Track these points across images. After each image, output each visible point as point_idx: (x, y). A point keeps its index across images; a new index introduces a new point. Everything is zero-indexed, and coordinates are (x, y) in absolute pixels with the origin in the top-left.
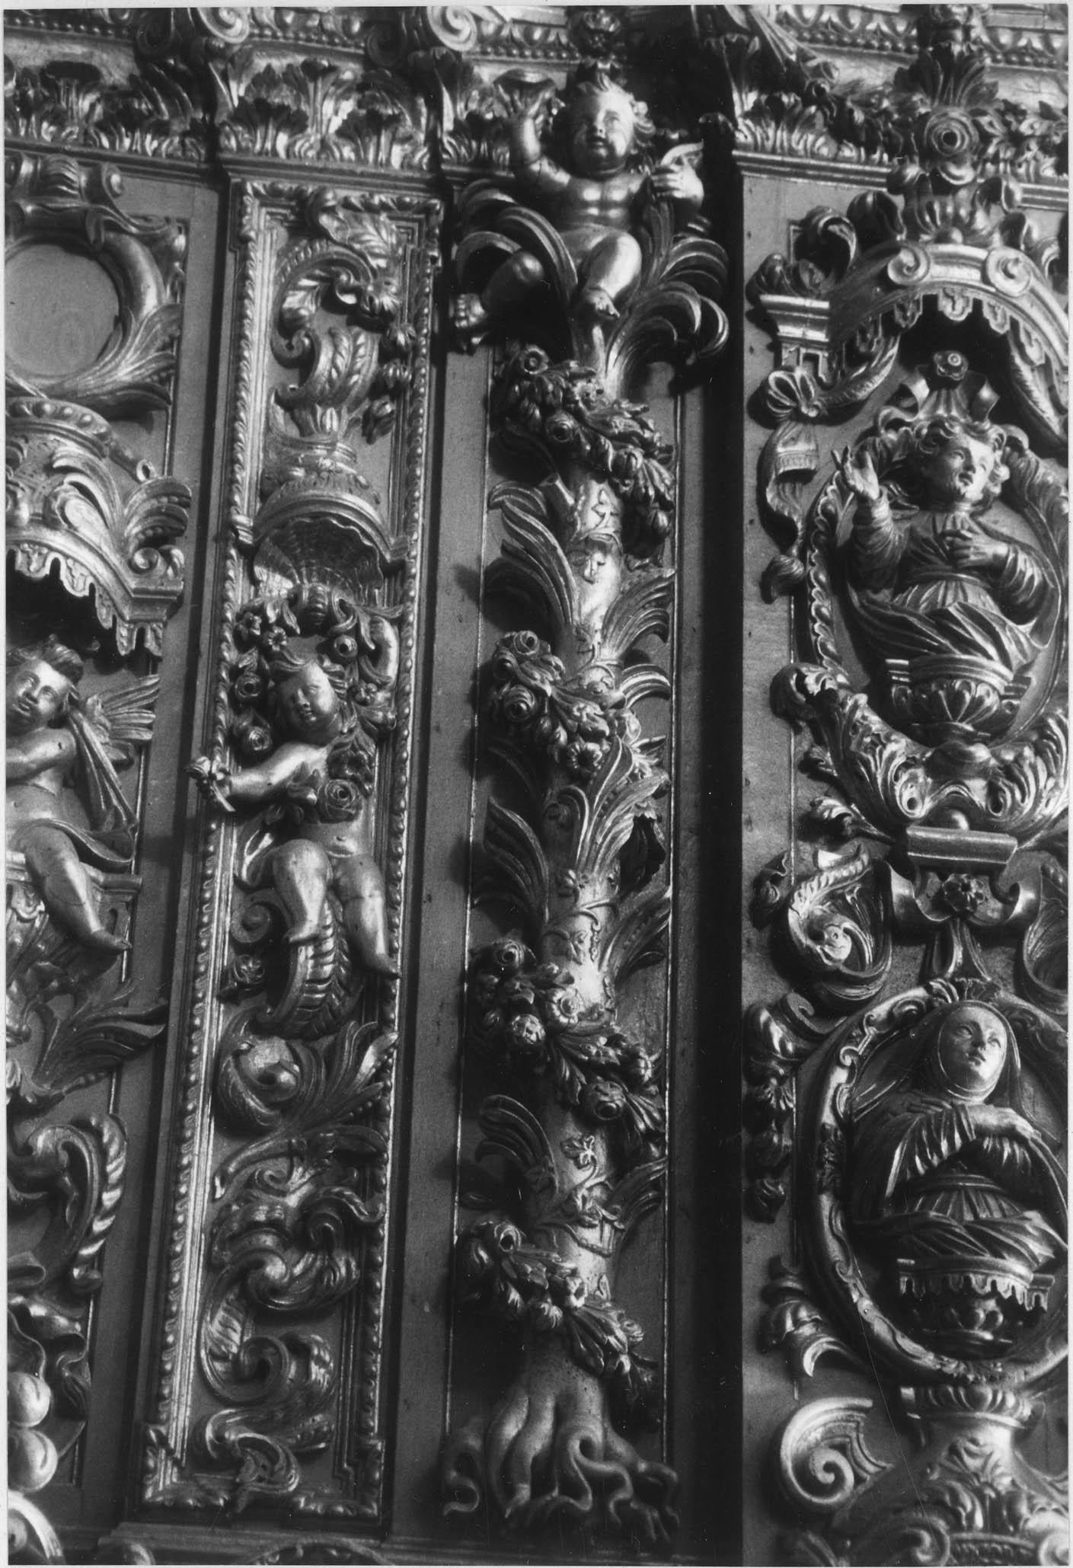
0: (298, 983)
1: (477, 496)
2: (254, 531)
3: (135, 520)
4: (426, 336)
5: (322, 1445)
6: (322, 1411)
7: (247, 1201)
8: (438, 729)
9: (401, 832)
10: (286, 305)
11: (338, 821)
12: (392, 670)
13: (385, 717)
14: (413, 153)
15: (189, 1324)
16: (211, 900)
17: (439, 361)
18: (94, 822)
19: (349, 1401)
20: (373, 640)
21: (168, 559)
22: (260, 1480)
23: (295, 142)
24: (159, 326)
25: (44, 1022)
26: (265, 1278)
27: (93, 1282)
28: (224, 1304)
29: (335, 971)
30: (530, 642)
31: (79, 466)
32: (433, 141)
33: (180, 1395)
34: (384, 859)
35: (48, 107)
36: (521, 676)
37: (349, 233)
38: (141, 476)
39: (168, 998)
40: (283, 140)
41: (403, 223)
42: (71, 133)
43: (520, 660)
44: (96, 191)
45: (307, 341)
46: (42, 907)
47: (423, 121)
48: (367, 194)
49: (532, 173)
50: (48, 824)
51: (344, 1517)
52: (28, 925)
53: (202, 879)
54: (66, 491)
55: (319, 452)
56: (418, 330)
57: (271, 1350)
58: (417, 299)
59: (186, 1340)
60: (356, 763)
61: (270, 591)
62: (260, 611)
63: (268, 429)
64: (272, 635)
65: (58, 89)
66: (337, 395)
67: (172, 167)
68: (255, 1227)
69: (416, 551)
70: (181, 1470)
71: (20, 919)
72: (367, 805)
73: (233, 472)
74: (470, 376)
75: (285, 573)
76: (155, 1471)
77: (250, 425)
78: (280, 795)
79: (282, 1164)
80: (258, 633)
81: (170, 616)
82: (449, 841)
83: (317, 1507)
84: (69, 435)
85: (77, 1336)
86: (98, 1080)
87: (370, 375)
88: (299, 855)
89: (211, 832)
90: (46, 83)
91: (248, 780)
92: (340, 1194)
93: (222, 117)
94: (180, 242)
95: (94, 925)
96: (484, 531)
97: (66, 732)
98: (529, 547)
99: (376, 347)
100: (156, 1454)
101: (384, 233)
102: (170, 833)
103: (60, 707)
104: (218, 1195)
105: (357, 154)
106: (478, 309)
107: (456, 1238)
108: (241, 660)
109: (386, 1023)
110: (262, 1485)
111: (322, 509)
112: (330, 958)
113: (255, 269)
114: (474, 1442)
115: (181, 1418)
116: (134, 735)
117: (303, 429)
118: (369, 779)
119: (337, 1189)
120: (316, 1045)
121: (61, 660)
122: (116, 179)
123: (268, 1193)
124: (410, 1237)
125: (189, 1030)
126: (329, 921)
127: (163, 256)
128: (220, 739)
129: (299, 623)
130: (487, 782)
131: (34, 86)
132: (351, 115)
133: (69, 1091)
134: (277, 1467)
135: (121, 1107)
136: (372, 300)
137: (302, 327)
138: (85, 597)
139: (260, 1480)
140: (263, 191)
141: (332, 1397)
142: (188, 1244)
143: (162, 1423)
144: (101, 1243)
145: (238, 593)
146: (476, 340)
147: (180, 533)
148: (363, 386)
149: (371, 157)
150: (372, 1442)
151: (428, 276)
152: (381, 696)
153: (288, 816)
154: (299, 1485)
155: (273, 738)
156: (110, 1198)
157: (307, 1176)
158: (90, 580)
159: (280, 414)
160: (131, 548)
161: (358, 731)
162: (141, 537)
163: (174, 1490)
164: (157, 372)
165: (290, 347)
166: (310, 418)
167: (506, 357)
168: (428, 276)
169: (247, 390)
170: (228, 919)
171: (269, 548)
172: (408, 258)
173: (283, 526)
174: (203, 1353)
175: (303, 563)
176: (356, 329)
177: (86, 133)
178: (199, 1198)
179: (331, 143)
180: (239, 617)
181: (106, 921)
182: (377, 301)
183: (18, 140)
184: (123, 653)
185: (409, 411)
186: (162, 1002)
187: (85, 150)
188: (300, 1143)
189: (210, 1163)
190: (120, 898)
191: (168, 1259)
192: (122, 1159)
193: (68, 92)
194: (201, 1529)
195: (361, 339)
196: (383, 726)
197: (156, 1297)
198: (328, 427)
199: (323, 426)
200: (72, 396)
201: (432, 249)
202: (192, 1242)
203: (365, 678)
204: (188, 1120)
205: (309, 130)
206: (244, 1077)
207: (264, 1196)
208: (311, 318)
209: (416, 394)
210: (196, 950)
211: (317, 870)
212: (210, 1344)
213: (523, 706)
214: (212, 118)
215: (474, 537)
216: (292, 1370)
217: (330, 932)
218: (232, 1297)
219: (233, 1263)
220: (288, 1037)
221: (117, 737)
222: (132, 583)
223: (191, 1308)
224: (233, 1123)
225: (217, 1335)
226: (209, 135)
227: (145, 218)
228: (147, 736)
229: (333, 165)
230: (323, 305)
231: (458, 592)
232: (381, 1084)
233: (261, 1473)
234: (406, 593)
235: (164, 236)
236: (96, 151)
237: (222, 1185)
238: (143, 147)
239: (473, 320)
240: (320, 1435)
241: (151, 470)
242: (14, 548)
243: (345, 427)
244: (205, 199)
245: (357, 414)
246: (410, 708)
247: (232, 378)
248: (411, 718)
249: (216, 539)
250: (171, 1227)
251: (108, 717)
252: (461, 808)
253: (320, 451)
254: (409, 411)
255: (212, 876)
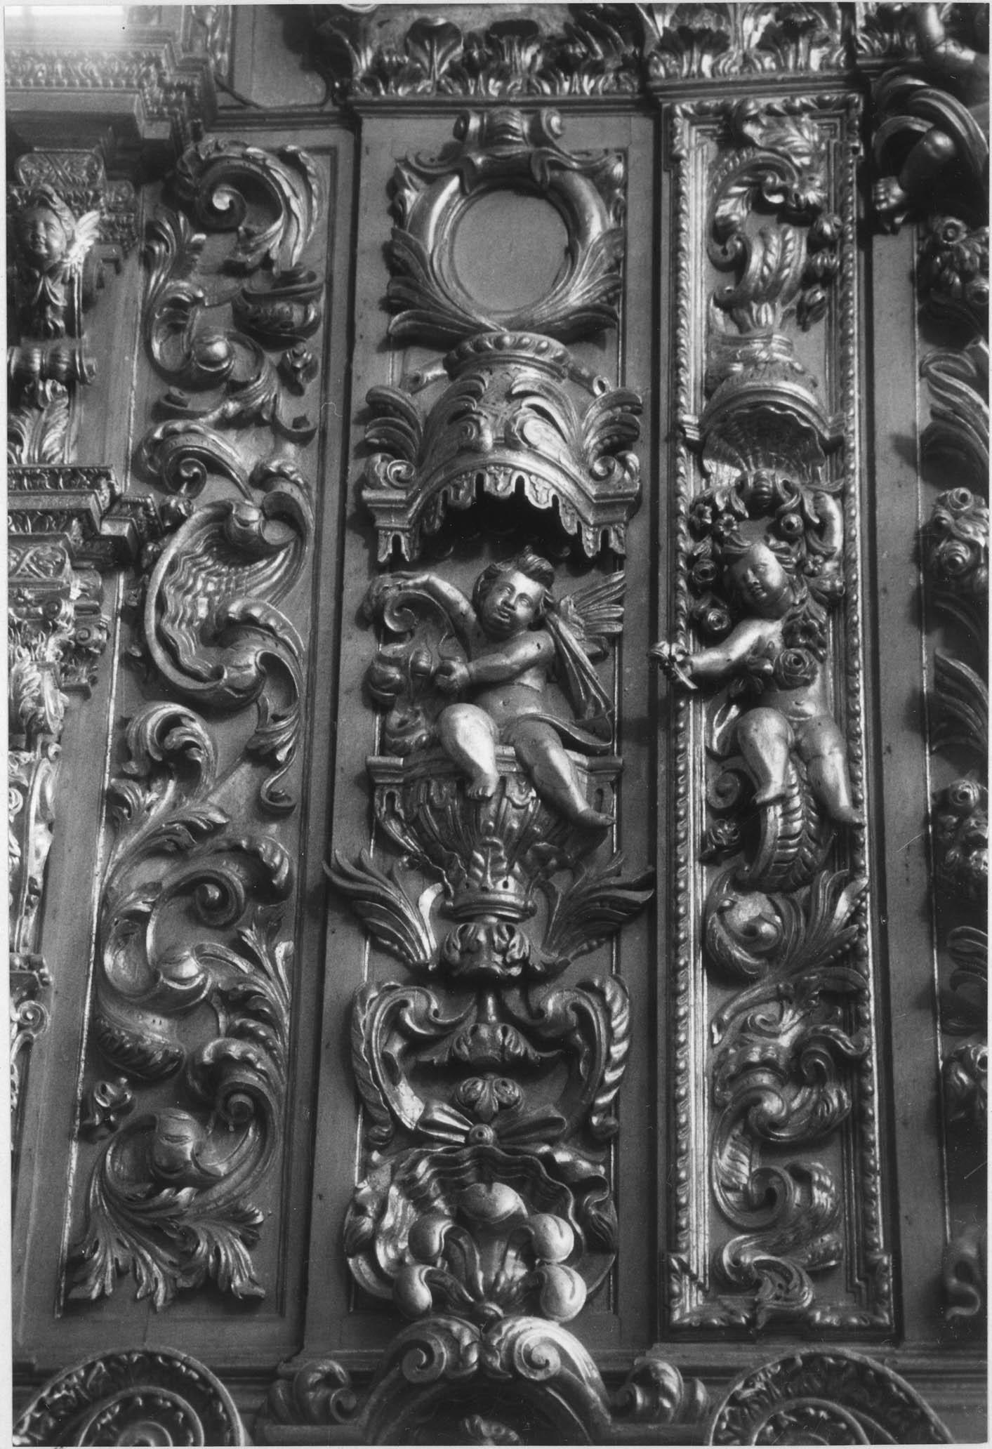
0: (769, 840)
1: (908, 366)
2: (700, 427)
3: (592, 432)
4: (851, 223)
5: (833, 1263)
6: (830, 1231)
7: (742, 1045)
8: (885, 591)
9: (857, 691)
10: (718, 214)
11: (796, 687)
12: (837, 541)
13: (833, 585)
14: (831, 54)
15: (701, 1160)
16: (686, 772)
17: (865, 244)
18: (577, 711)
19: (854, 1221)
20: (817, 515)
21: (624, 463)
22: (777, 1298)
23: (718, 62)
24: (603, 251)
25: (547, 896)
26: (763, 1113)
27: (609, 1128)
28: (730, 1140)
29: (804, 826)
30: (964, 498)
31: (536, 389)
32: (849, 41)
33: (698, 1226)
34: (844, 719)
35: (493, 65)
36: (955, 531)
37: (773, 137)
38: (597, 390)
39: (655, 865)
40: (707, 61)
41: (826, 121)
42: (516, 85)
43: (956, 516)
44: (538, 135)
45: (739, 245)
46: (533, 793)
47: (839, 22)
48: (788, 98)
49: (938, 56)
50: (534, 718)
51: (859, 1328)
52: (522, 811)
53: (676, 753)
54: (525, 414)
55: (756, 346)
56: (844, 219)
57: (776, 1179)
58: (842, 190)
59: (698, 1175)
60: (808, 631)
61: (721, 482)
62: (710, 501)
63: (710, 330)
64: (722, 522)
65: (501, 47)
66: (771, 290)
67: (608, 102)
68: (749, 1068)
69: (855, 426)
70: (706, 1293)
71: (515, 806)
72: (824, 670)
73: (678, 375)
74: (895, 254)
75: (733, 463)
76: (680, 1295)
77: (692, 329)
78: (740, 669)
79: (773, 1008)
80: (709, 521)
81: (631, 516)
82: (904, 693)
83: (832, 1320)
84: (529, 362)
85: (599, 1178)
86: (600, 945)
87: (800, 266)
88: (759, 722)
89: (680, 710)
90: (491, 43)
91: (709, 659)
92: (827, 1031)
93: (650, 48)
94: (618, 169)
95: (581, 805)
96: (918, 399)
97: (543, 633)
98: (957, 410)
99: (804, 239)
100: (680, 1280)
101: (806, 133)
102: (645, 715)
103: (537, 612)
104: (716, 1041)
105: (778, 64)
106: (897, 191)
107: (941, 1063)
108: (695, 549)
109: (857, 870)
110: (780, 1302)
111: (759, 399)
112: (799, 814)
113: (687, 184)
114: (971, 1251)
115: (701, 1246)
116: (606, 629)
117: (742, 327)
118: (823, 645)
119: (824, 1027)
120: (795, 896)
121: (533, 568)
122: (555, 121)
123: (761, 1035)
124: (897, 1066)
125: (675, 892)
126: (794, 781)
127: (604, 185)
128: (682, 623)
129: (747, 507)
130: (937, 636)
131: (480, 47)
132: (769, 27)
133: (574, 958)
134: (792, 1283)
135: (622, 967)
136: (797, 197)
137: (733, 231)
138: (549, 509)
139: (777, 1298)
140: (691, 111)
141: (839, 1218)
142: (692, 1089)
143: (682, 1251)
144: (614, 1092)
145: (690, 487)
146: (899, 220)
147: (635, 438)
148: (794, 278)
149: (791, 64)
150: (878, 1257)
151: (851, 166)
152: (829, 566)
153: (750, 687)
154: (813, 1301)
155: (731, 616)
156: (618, 1050)
157: (797, 1017)
158: (553, 492)
159: (719, 315)
160: (591, 458)
161: (810, 603)
162: (600, 446)
163: (701, 1312)
164: (605, 293)
165: (725, 252)
166: (747, 315)
167: (929, 231)
168: (851, 166)
169: (687, 298)
170: (704, 788)
171: (716, 442)
172: (832, 152)
173: (724, 420)
174: (715, 1186)
175: (748, 451)
176: (785, 226)
177: (529, 84)
178: (699, 1046)
179: (752, 57)
180: (692, 509)
181: (594, 801)
182: (802, 197)
183: (470, 99)
184: (590, 555)
185: (840, 296)
186: (650, 868)
187: (530, 99)
188: (787, 987)
189: (706, 1012)
190: (605, 779)
191: (675, 1102)
192: (626, 1012)
193: (511, 48)
194: (727, 1345)
195: (790, 235)
196: (832, 593)
197: (668, 1137)
198: (764, 321)
199: (759, 321)
200: (531, 326)
201: (854, 141)
202: (696, 1086)
203: (812, 551)
204: (680, 976)
205: (731, 48)
206: (729, 931)
207: (756, 1038)
208: (742, 223)
209: (846, 280)
210: (675, 820)
211: (779, 735)
212: (721, 1177)
213: (959, 559)
214: (641, 52)
215: (907, 408)
216: (797, 1196)
217: (796, 790)
218: (737, 1132)
219: (735, 1101)
220: (769, 891)
221: (591, 634)
222: (592, 490)
223: (700, 1145)
224: (723, 974)
225: (727, 1169)
226: (639, 67)
227: (587, 153)
228: (618, 628)
229: (755, 77)
230: (753, 207)
231: (895, 459)
232: (856, 927)
233: (778, 1291)
234: (846, 467)
235: (605, 166)
236: (538, 98)
237: (719, 1030)
238: (581, 87)
239: (893, 201)
240: (829, 1255)
241: (606, 383)
242: (481, 471)
243: (780, 319)
244: (640, 126)
245: (792, 305)
246: (858, 574)
247: (672, 289)
248: (860, 583)
249: (667, 440)
250: (675, 1073)
251: (580, 615)
252: (913, 661)
253: (757, 345)
254: (840, 296)
255: (685, 750)
